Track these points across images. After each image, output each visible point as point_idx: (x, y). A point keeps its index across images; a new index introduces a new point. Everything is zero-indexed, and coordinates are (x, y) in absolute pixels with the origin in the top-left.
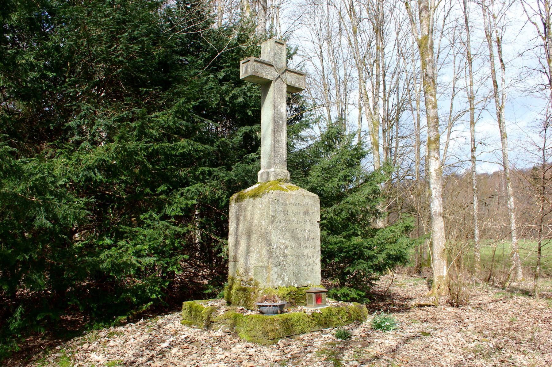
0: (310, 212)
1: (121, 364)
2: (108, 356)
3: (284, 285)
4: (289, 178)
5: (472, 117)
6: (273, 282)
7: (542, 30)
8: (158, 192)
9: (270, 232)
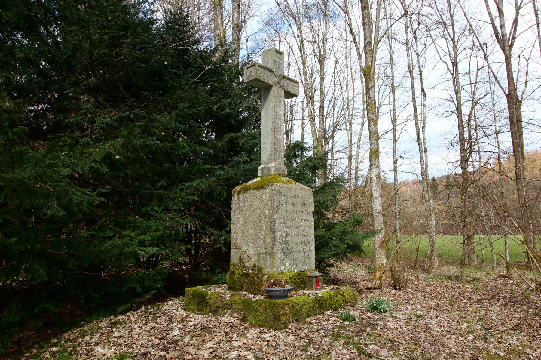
0: (306, 203)
1: (131, 357)
2: (114, 348)
3: (286, 271)
4: (286, 173)
5: (395, 136)
6: (277, 267)
7: (451, 68)
8: (157, 187)
9: (275, 221)
